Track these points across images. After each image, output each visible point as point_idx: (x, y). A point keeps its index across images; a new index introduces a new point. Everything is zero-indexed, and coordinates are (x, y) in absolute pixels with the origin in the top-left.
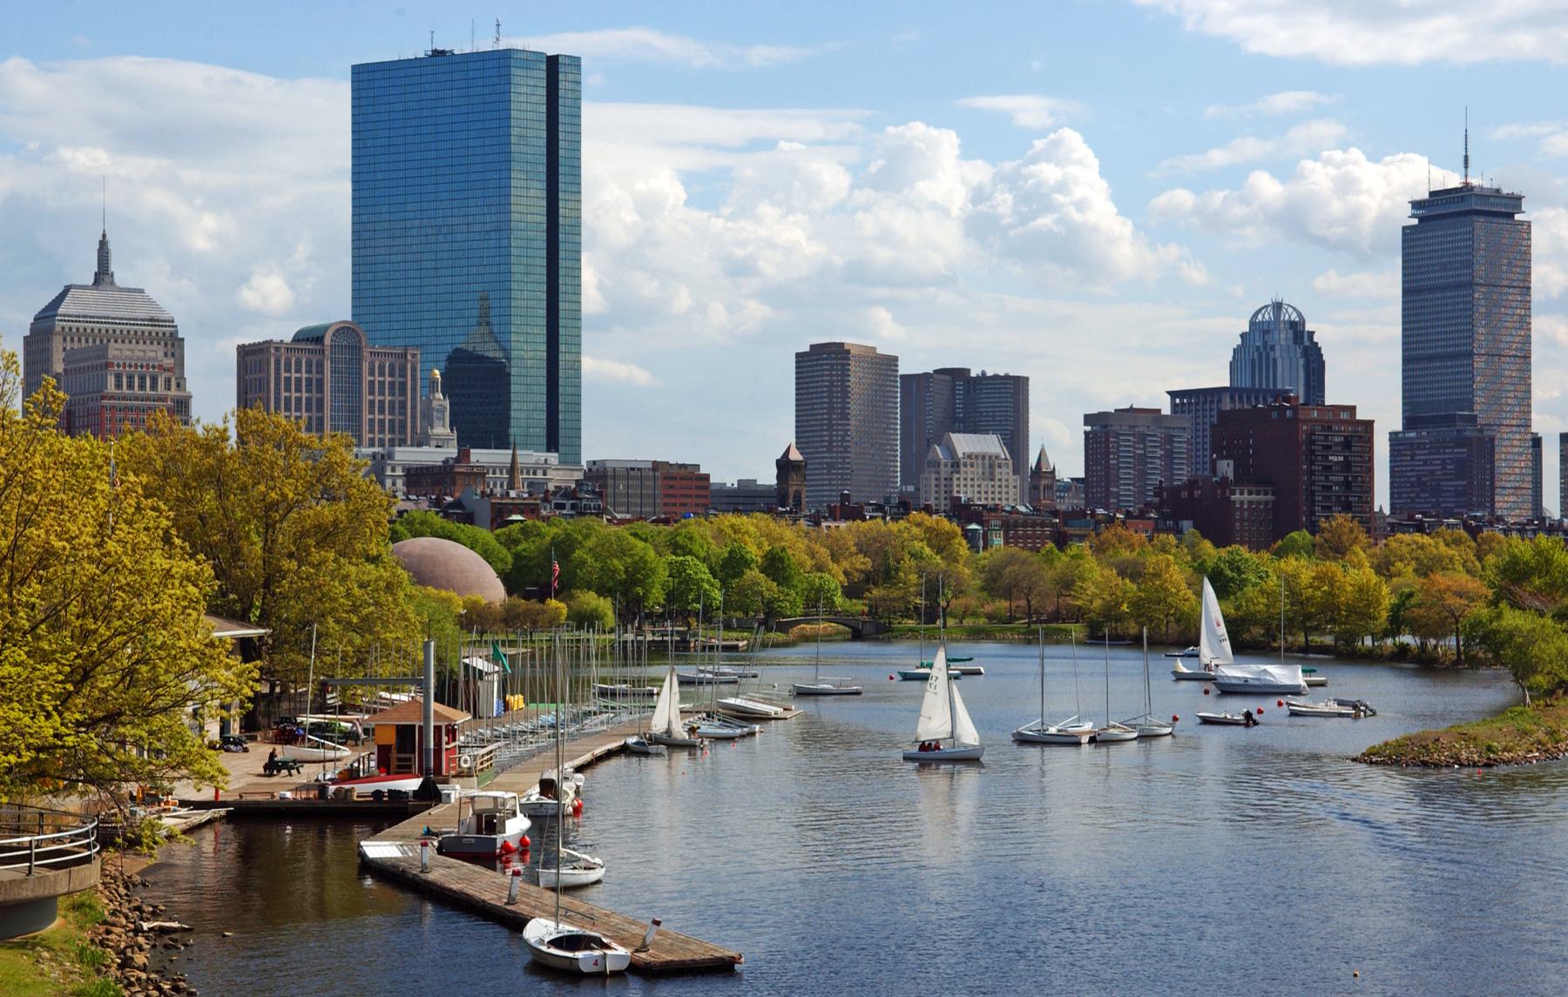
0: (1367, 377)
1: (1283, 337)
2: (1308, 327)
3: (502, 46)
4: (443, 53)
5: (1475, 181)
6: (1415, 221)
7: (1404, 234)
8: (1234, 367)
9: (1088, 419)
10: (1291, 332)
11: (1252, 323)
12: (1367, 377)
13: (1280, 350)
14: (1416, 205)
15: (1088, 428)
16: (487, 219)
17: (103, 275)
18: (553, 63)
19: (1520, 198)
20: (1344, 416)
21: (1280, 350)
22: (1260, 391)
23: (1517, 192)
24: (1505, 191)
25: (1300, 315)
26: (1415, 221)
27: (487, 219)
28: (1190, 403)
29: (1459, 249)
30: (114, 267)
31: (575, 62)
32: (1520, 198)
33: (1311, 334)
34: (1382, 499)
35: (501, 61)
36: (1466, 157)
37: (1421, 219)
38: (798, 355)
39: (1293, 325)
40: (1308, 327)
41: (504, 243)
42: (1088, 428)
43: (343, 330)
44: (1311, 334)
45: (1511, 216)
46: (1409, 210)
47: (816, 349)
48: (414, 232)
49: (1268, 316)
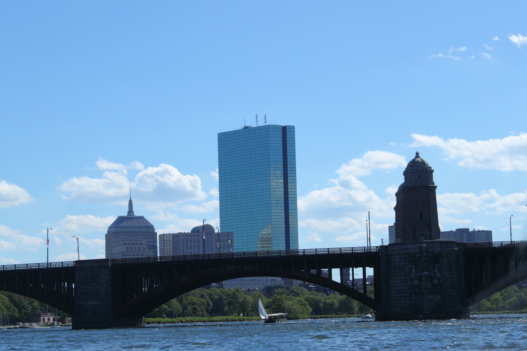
3: (267, 124)
4: (248, 127)
16: (263, 185)
17: (131, 211)
18: (284, 129)
27: (263, 185)
30: (134, 209)
31: (293, 128)
35: (267, 129)
38: (389, 227)
41: (269, 193)
48: (239, 190)
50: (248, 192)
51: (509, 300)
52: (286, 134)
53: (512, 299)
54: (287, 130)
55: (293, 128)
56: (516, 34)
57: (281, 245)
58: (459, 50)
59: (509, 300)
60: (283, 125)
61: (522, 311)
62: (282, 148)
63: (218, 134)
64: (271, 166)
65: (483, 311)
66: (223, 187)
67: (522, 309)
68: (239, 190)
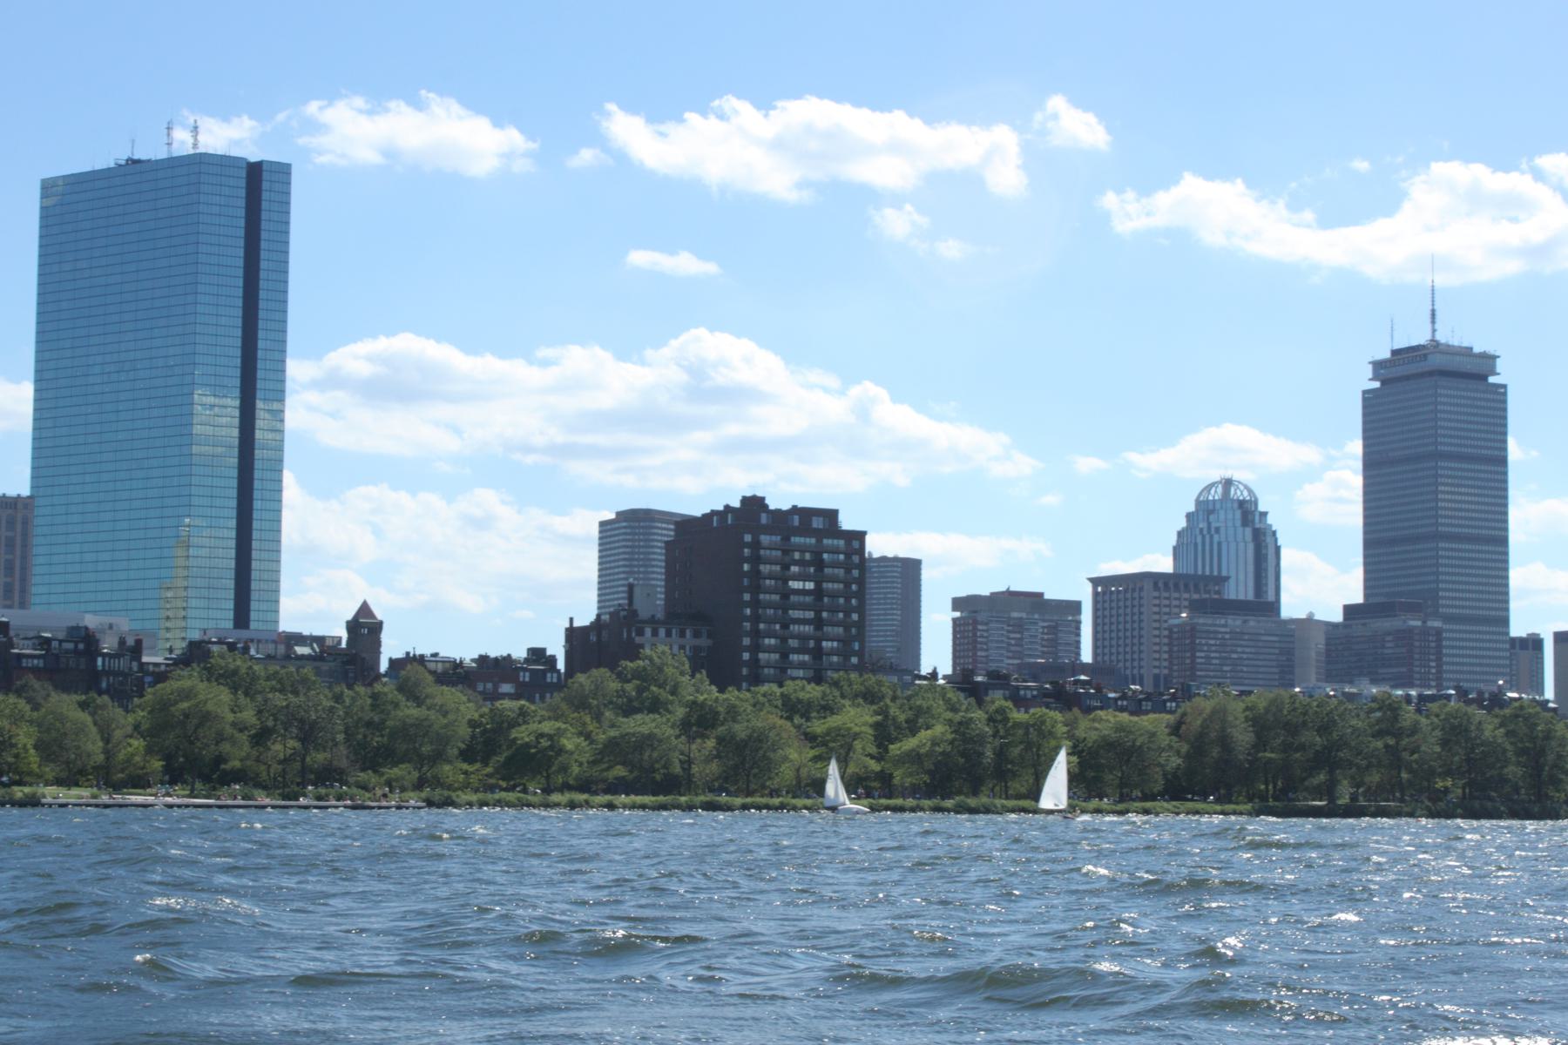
0: (1321, 580)
1: (1228, 520)
2: (1261, 508)
5: (1442, 337)
6: (1377, 385)
7: (1364, 400)
8: (1177, 552)
9: (958, 603)
10: (1238, 514)
11: (1198, 502)
12: (1321, 580)
13: (1231, 533)
14: (1378, 366)
15: (958, 614)
19: (1494, 358)
20: (817, 523)
21: (1231, 533)
22: (1204, 577)
23: (1491, 350)
24: (1477, 350)
25: (1250, 491)
26: (1377, 385)
28: (1126, 591)
29: (1432, 425)
31: (284, 170)
32: (1494, 358)
33: (1264, 514)
34: (1404, 670)
36: (1433, 322)
37: (1383, 383)
38: (602, 524)
39: (1242, 503)
40: (1261, 508)
42: (958, 614)
43: (1507, 633)
44: (1264, 514)
45: (1485, 378)
46: (1368, 371)
47: (624, 516)
48: (97, 370)
49: (1216, 494)
50: (123, 377)
51: (910, 743)
52: (258, 189)
53: (924, 735)
54: (265, 176)
55: (284, 170)
56: (1079, 102)
57: (220, 552)
58: (1062, 759)
59: (910, 743)
60: (253, 160)
61: (972, 802)
62: (242, 233)
63: (43, 181)
64: (201, 288)
65: (774, 793)
66: (47, 355)
67: (975, 793)
68: (97, 370)
